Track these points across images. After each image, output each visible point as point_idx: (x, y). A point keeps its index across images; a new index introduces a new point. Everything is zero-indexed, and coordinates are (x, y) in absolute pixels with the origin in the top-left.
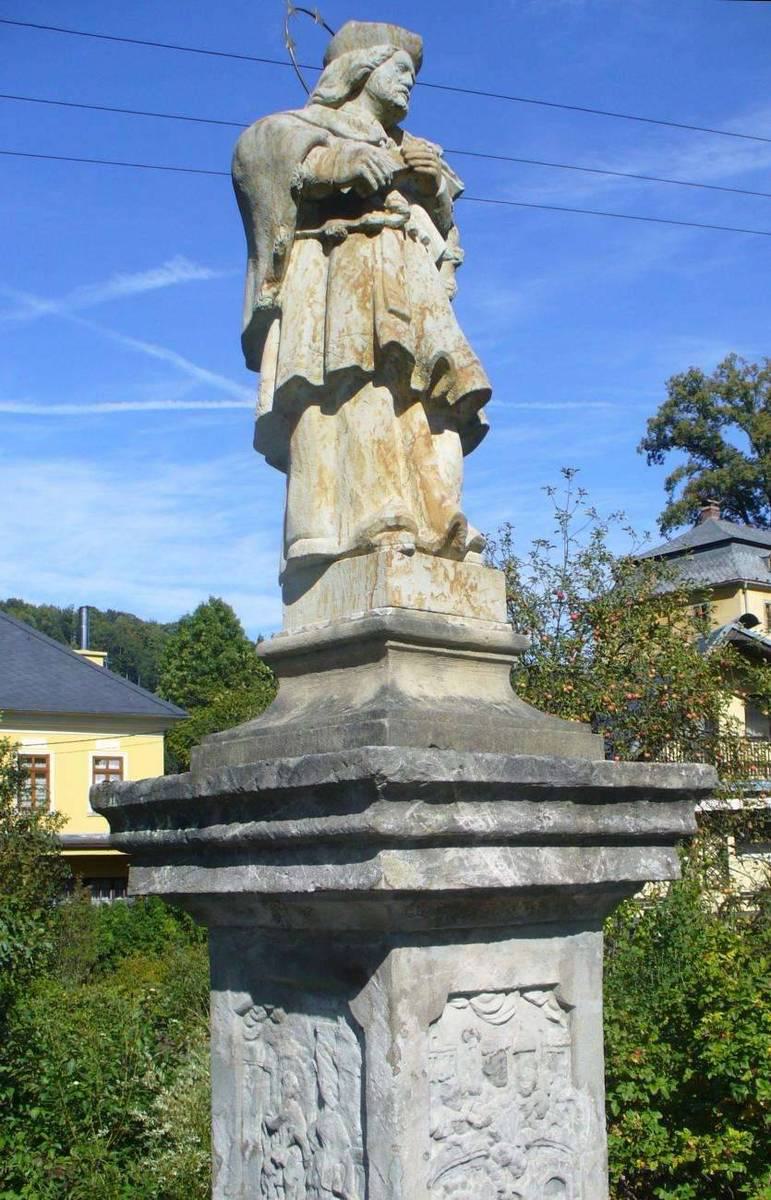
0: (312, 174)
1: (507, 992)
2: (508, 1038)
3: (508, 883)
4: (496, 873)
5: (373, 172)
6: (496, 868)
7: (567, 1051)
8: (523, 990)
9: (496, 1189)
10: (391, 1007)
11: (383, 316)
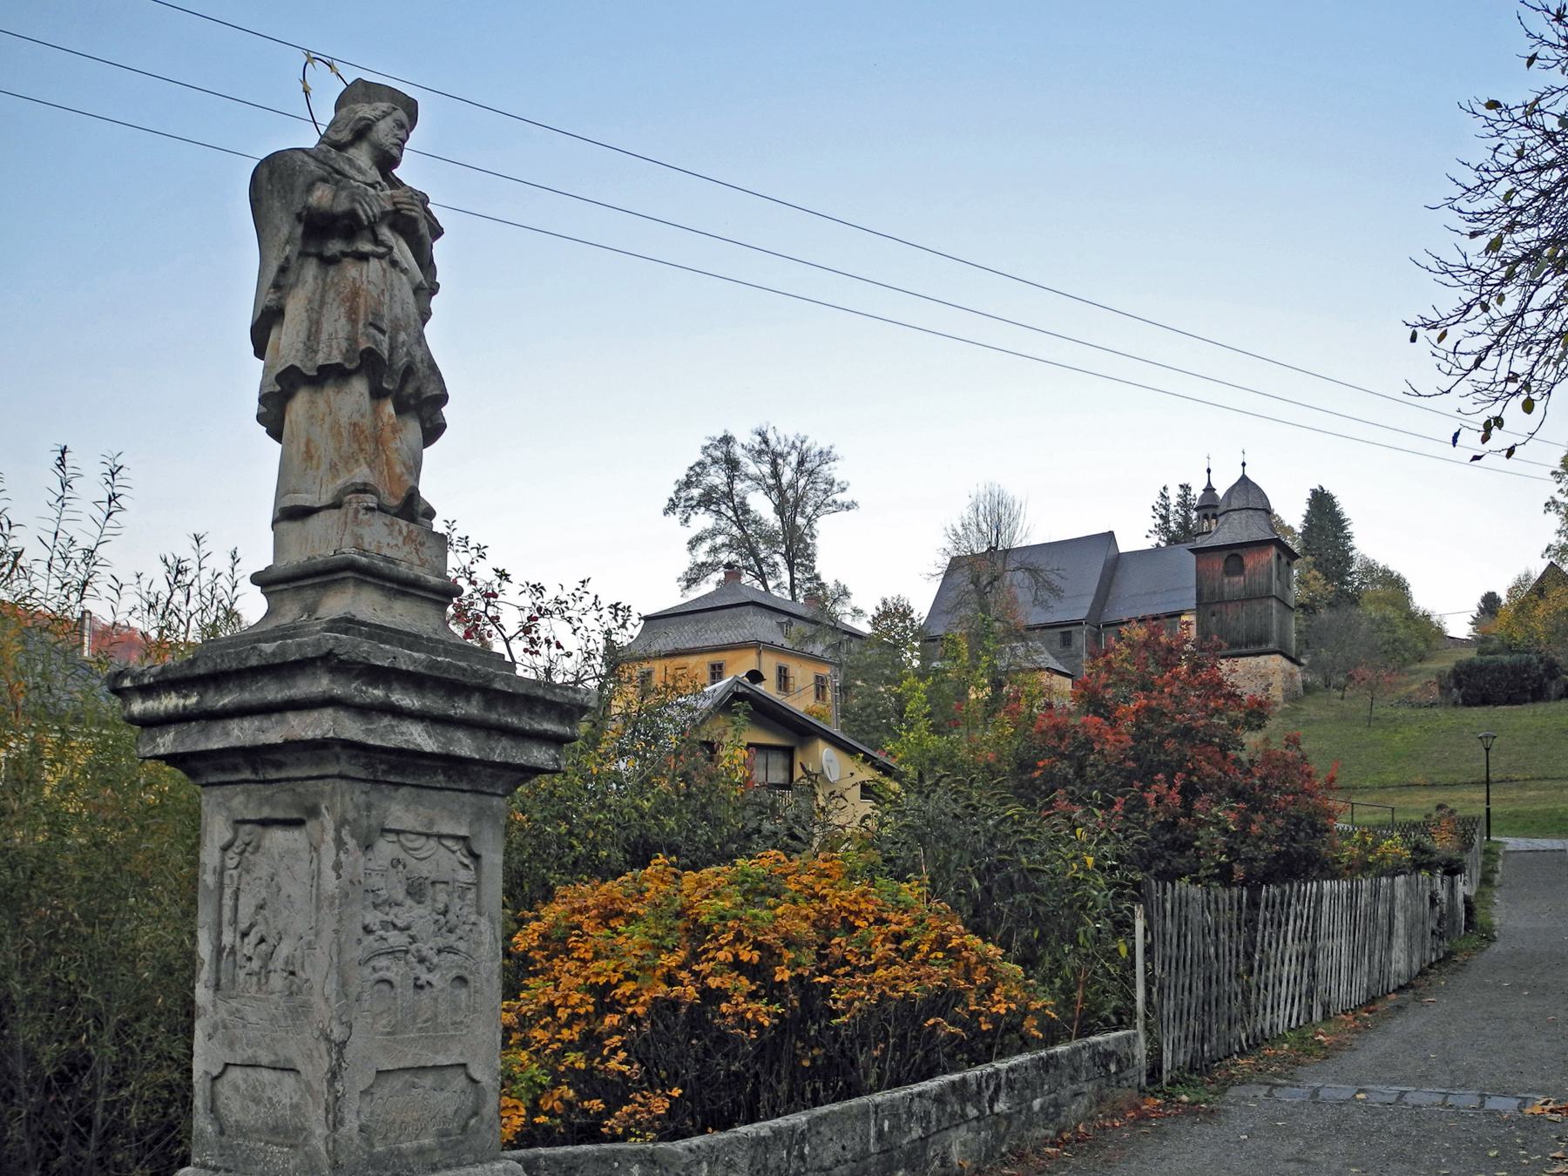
1: (428, 836)
2: (425, 870)
3: (428, 749)
4: (419, 740)
5: (365, 211)
6: (420, 738)
7: (474, 890)
8: (440, 836)
9: (413, 976)
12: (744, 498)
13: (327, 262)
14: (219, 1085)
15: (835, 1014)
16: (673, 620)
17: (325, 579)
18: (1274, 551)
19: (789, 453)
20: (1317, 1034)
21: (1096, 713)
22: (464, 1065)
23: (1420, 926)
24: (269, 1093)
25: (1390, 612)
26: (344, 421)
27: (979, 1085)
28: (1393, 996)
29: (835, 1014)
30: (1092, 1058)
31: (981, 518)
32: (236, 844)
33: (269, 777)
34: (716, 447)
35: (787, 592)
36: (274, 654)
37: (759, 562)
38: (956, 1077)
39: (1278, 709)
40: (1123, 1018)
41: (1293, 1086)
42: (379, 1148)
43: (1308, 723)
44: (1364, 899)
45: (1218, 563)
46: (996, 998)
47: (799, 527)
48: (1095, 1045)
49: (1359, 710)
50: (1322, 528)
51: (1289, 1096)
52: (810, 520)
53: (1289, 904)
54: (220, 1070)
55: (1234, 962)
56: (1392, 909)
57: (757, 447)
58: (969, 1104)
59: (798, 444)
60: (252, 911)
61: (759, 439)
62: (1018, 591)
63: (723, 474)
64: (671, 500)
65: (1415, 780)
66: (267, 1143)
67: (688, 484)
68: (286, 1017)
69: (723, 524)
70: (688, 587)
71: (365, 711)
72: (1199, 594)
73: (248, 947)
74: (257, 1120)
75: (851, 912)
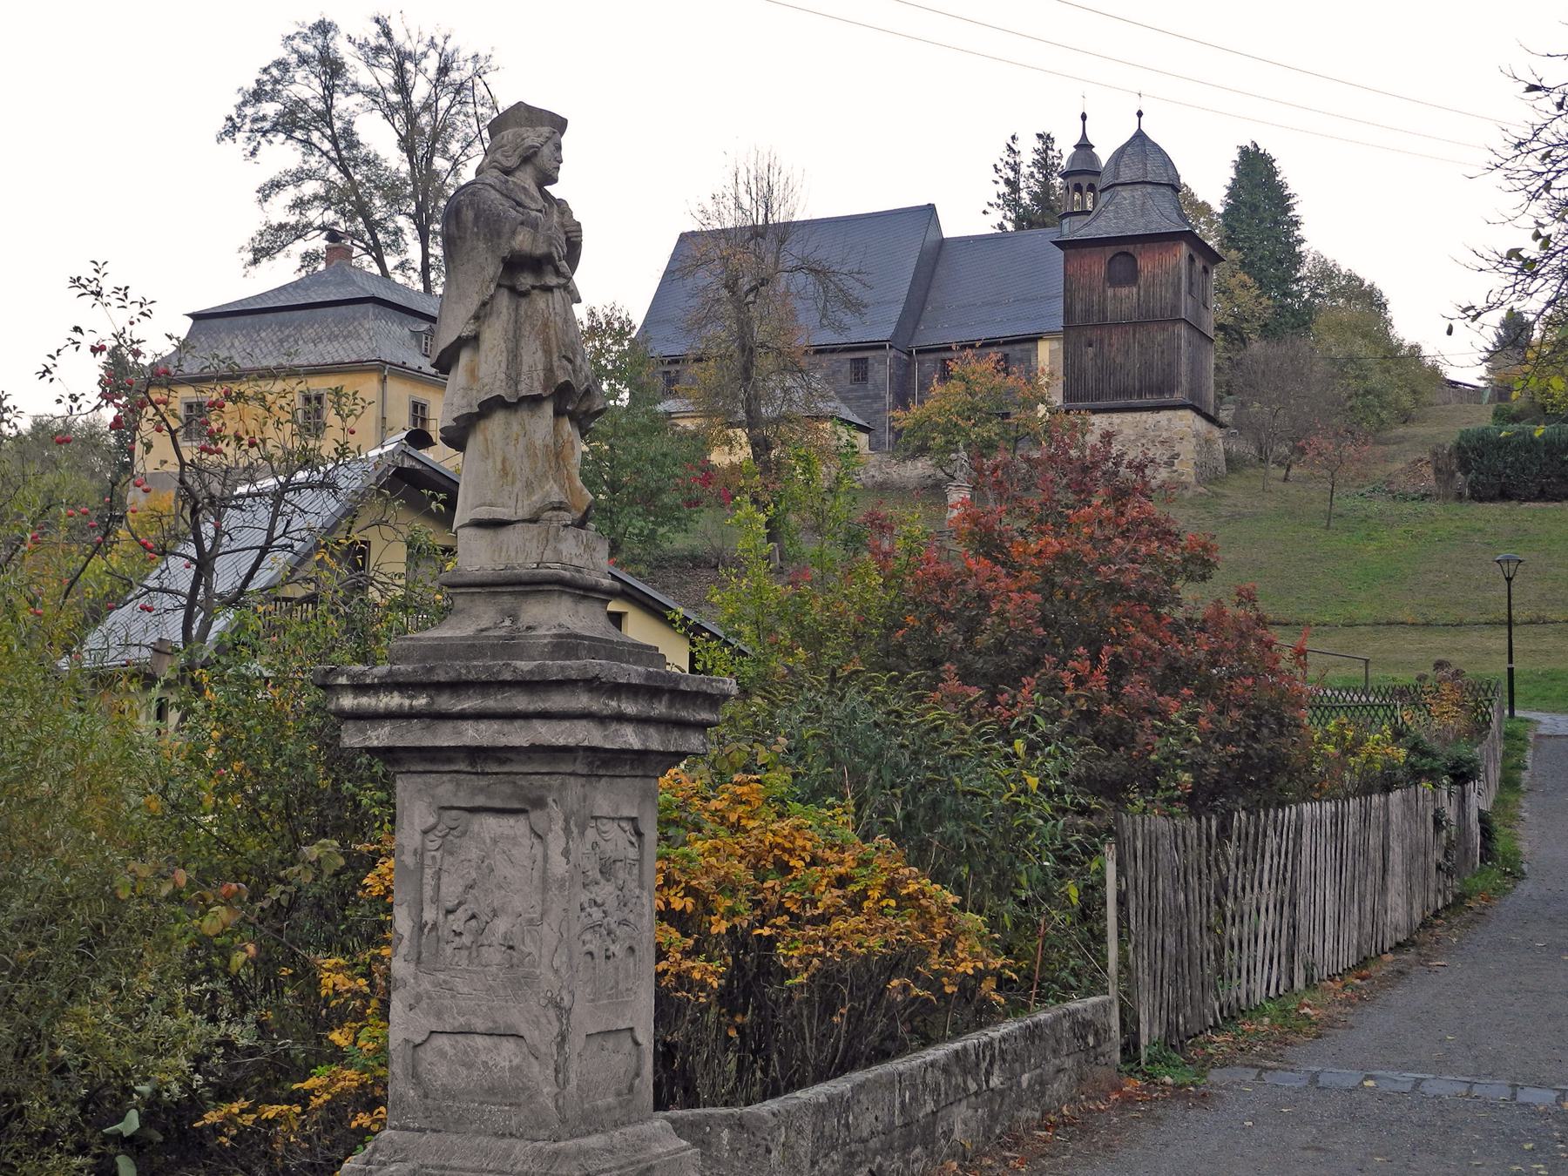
1: (613, 819)
2: (609, 849)
12: (350, 123)
13: (517, 293)
14: (420, 1051)
15: (786, 974)
16: (241, 320)
17: (528, 588)
18: (1184, 249)
19: (425, 55)
20: (1303, 1005)
21: (987, 555)
22: (631, 1029)
23: (1421, 859)
25: (1360, 347)
26: (539, 443)
27: (977, 1055)
28: (1389, 957)
29: (786, 974)
30: (1072, 1029)
31: (742, 188)
32: (439, 828)
33: (487, 770)
34: (305, 38)
35: (415, 276)
36: (531, 672)
37: (372, 226)
38: (957, 1045)
39: (1188, 494)
40: (1098, 987)
41: (1285, 1070)
42: (586, 1106)
43: (1235, 517)
44: (1352, 824)
45: (1097, 265)
46: (961, 955)
47: (438, 174)
48: (1072, 1014)
49: (1312, 501)
50: (1254, 208)
51: (1291, 1081)
52: (455, 164)
53: (1265, 835)
54: (424, 1038)
55: (1204, 911)
56: (1386, 837)
57: (373, 43)
58: (969, 1077)
59: (439, 41)
60: (460, 889)
61: (377, 28)
62: (798, 304)
63: (316, 83)
64: (230, 119)
65: (1400, 618)
66: (481, 1103)
67: (258, 96)
68: (505, 988)
69: (314, 161)
70: (255, 261)
71: (601, 719)
72: (1068, 312)
73: (457, 921)
74: (469, 1083)
75: (784, 850)
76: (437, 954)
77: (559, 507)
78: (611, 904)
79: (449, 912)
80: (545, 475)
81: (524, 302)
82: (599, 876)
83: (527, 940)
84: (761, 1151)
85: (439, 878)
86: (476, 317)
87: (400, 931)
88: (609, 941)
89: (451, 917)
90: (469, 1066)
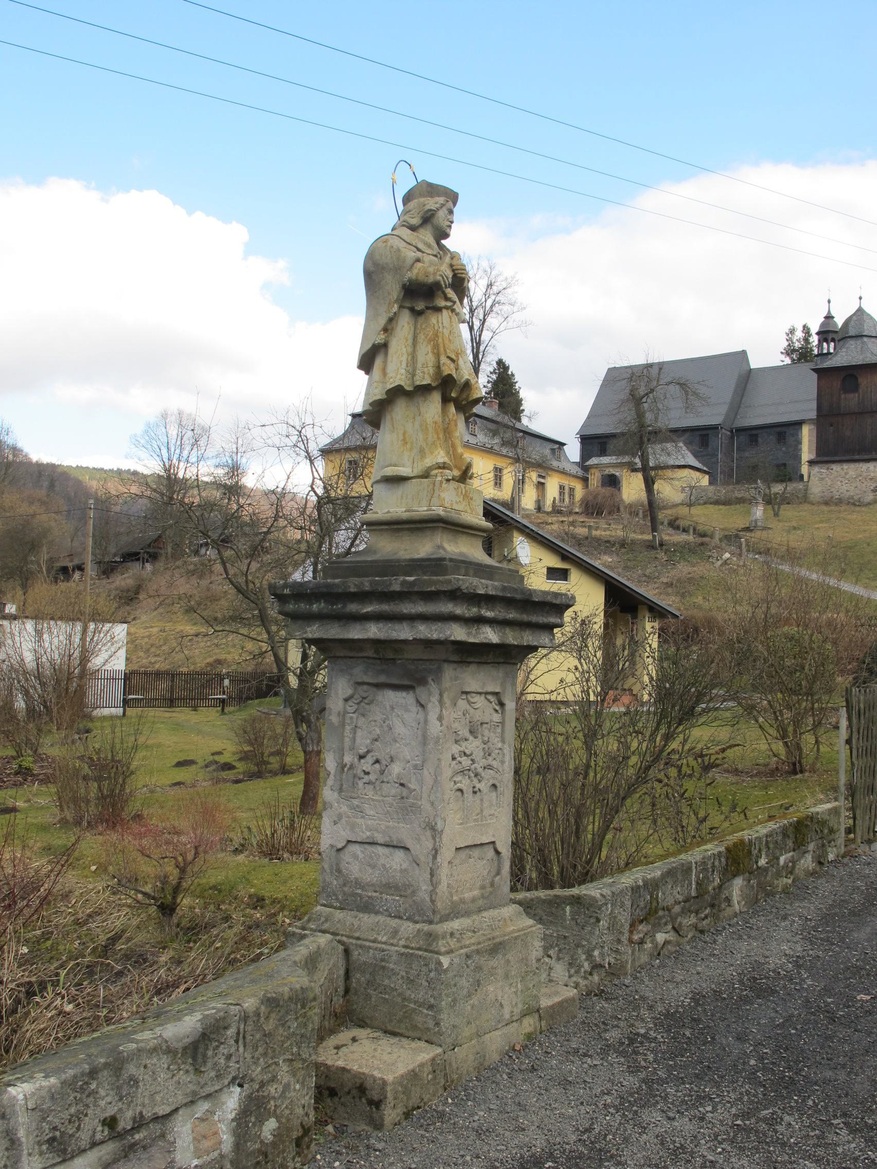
0: (414, 277)
1: (480, 693)
2: (478, 716)
3: (494, 642)
10: (441, 695)
11: (443, 359)
14: (341, 854)
22: (493, 843)
24: (382, 861)
26: (429, 421)
32: (355, 697)
33: (338, 654)
42: (455, 898)
54: (343, 844)
66: (381, 893)
73: (366, 764)
76: (354, 785)
77: (443, 466)
78: (478, 754)
79: (362, 757)
80: (434, 443)
81: (421, 320)
82: (468, 735)
83: (413, 780)
84: (592, 920)
85: (355, 733)
86: (385, 330)
87: (329, 769)
88: (475, 780)
89: (362, 761)
90: (373, 867)
